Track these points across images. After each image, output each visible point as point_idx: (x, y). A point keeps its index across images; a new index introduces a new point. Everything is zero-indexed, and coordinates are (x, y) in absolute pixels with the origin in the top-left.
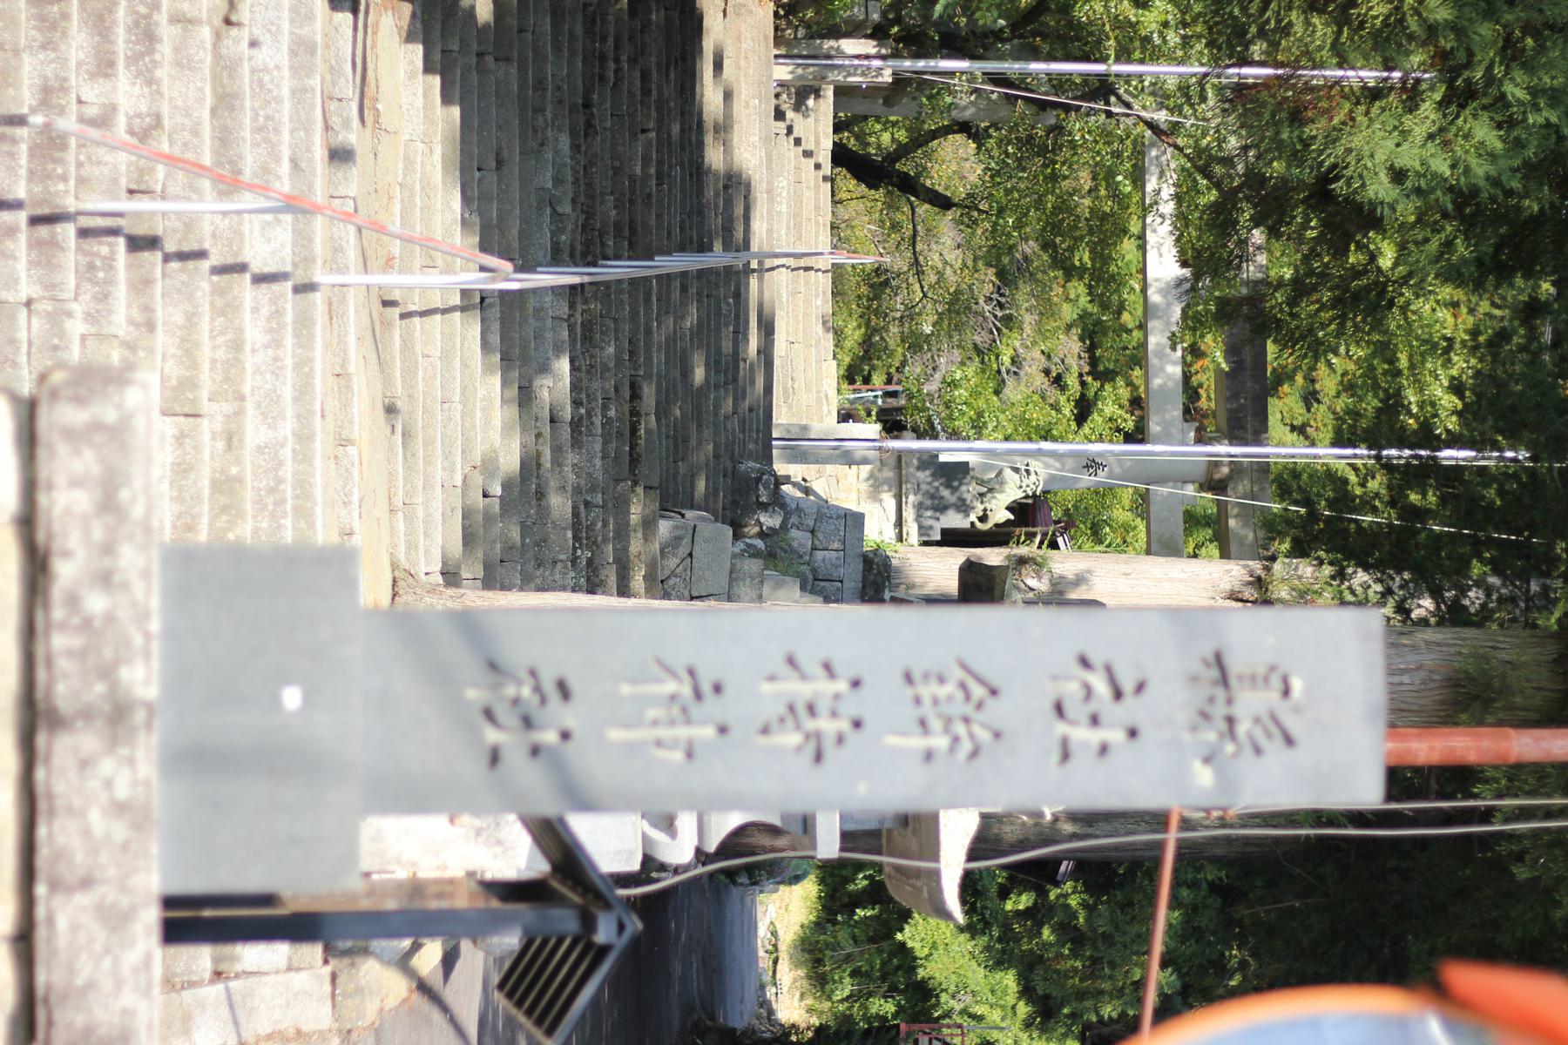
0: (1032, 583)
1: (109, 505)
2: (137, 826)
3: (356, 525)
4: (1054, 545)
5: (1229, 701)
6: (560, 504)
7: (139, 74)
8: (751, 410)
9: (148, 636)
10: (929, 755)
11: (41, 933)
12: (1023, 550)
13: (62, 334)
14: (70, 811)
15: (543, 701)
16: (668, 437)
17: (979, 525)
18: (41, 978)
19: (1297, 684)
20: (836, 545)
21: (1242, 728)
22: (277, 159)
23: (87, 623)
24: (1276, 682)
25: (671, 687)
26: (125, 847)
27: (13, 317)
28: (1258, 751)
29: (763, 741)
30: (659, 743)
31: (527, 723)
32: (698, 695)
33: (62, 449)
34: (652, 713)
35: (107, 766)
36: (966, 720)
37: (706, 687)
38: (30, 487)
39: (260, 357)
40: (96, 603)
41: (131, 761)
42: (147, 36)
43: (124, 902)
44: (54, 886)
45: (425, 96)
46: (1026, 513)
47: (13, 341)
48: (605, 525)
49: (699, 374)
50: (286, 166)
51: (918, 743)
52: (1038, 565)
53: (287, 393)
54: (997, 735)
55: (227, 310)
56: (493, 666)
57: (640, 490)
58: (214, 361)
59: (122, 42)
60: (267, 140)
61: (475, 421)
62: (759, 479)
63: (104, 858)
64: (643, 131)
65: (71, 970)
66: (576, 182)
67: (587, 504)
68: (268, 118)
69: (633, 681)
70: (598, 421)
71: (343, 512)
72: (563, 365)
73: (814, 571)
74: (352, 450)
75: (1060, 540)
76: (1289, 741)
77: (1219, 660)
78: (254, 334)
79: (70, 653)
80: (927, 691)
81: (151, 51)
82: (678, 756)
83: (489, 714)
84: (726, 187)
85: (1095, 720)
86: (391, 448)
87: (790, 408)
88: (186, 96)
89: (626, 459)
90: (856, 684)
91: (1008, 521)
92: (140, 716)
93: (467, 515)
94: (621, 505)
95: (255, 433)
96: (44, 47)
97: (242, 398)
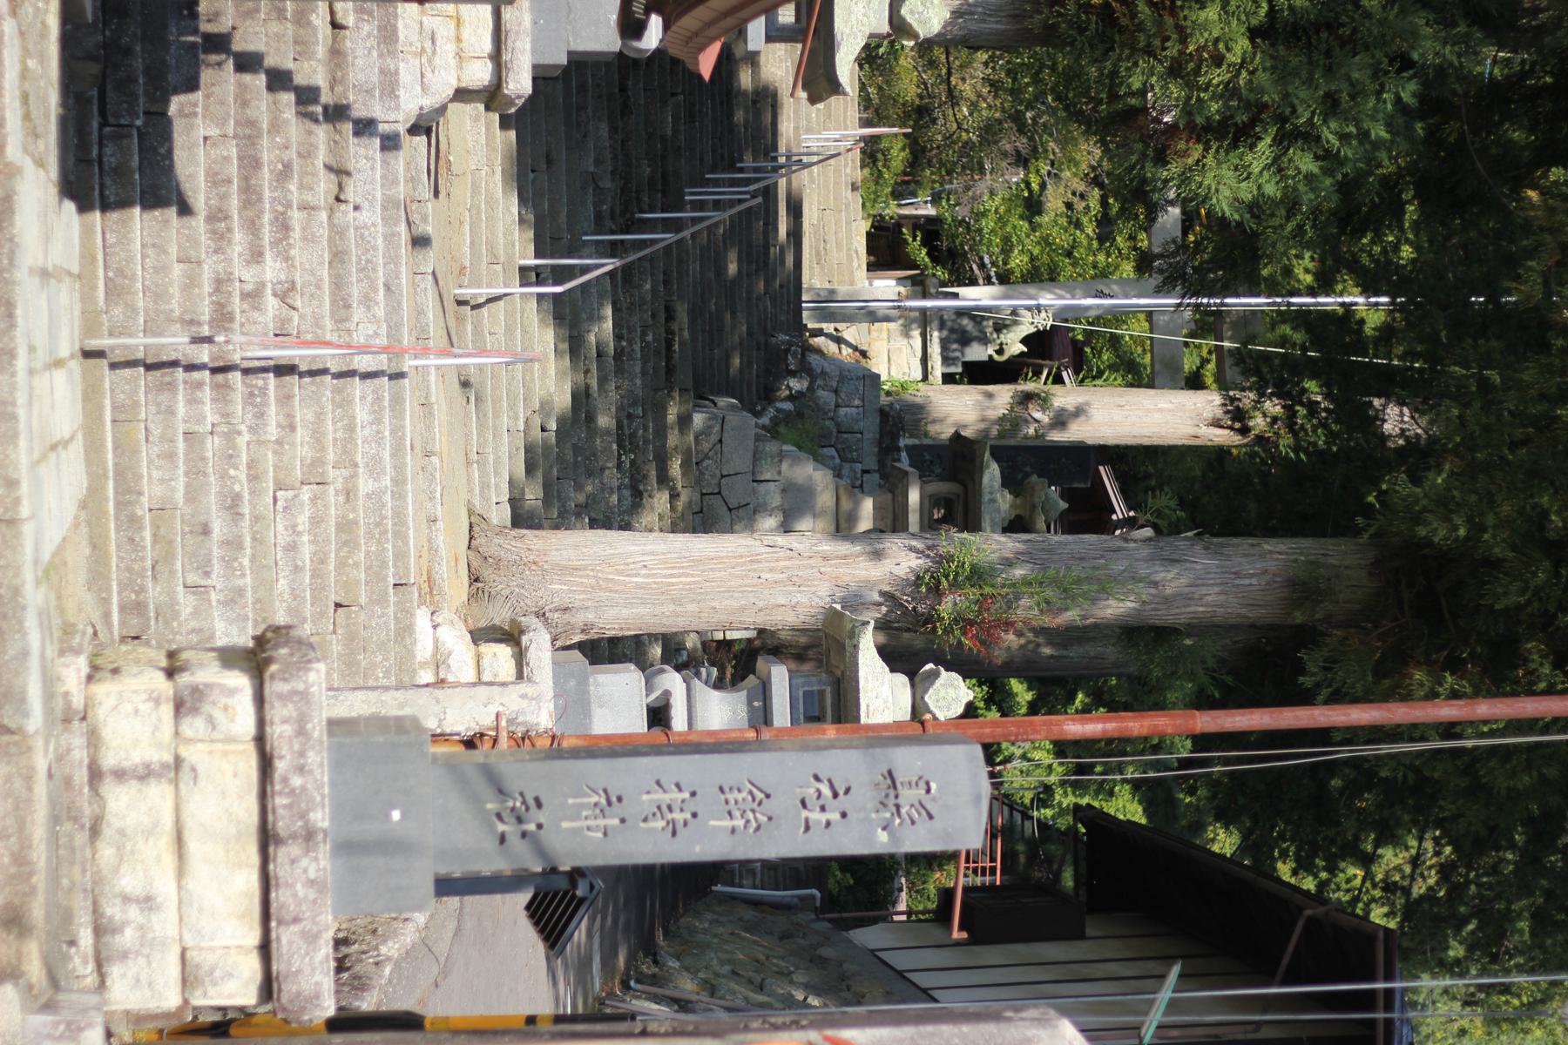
0: (1038, 415)
1: (301, 732)
2: (320, 892)
3: (439, 513)
4: (1058, 380)
5: (897, 797)
6: (604, 421)
7: (279, 253)
8: (781, 286)
9: (323, 796)
10: (733, 831)
11: (274, 945)
12: (1030, 386)
13: (235, 447)
14: (287, 885)
15: (527, 809)
16: (703, 331)
17: (996, 357)
18: (274, 968)
19: (933, 786)
20: (857, 402)
21: (903, 811)
22: (376, 290)
23: (293, 791)
24: (922, 784)
25: (595, 799)
26: (314, 902)
27: (202, 442)
28: (913, 822)
29: (643, 825)
30: (589, 829)
31: (520, 820)
32: (609, 803)
33: (277, 704)
34: (584, 813)
35: (305, 862)
36: (753, 811)
37: (614, 799)
38: (261, 723)
39: (367, 431)
40: (297, 781)
41: (316, 859)
42: (284, 226)
43: (315, 929)
44: (280, 923)
45: (487, 129)
46: (1039, 343)
47: (203, 459)
48: (645, 428)
49: (732, 268)
50: (382, 292)
51: (727, 823)
52: (1043, 400)
53: (387, 455)
54: (770, 819)
55: (344, 403)
56: (500, 791)
57: (676, 394)
58: (335, 440)
59: (267, 235)
60: (367, 277)
61: (531, 370)
62: (787, 351)
63: (304, 908)
64: (673, 95)
65: (289, 963)
66: (615, 157)
67: (629, 416)
68: (368, 261)
69: (575, 797)
70: (637, 348)
71: (429, 505)
72: (608, 311)
73: (838, 425)
74: (435, 460)
75: (1064, 374)
76: (931, 817)
77: (890, 772)
78: (362, 414)
79: (285, 807)
80: (731, 797)
81: (286, 237)
82: (600, 835)
83: (499, 816)
84: (754, 102)
85: (823, 809)
86: (467, 415)
87: (822, 268)
88: (311, 259)
89: (663, 372)
90: (693, 794)
91: (1022, 353)
92: (320, 837)
93: (529, 449)
94: (660, 410)
95: (365, 485)
96: (216, 252)
97: (356, 465)
